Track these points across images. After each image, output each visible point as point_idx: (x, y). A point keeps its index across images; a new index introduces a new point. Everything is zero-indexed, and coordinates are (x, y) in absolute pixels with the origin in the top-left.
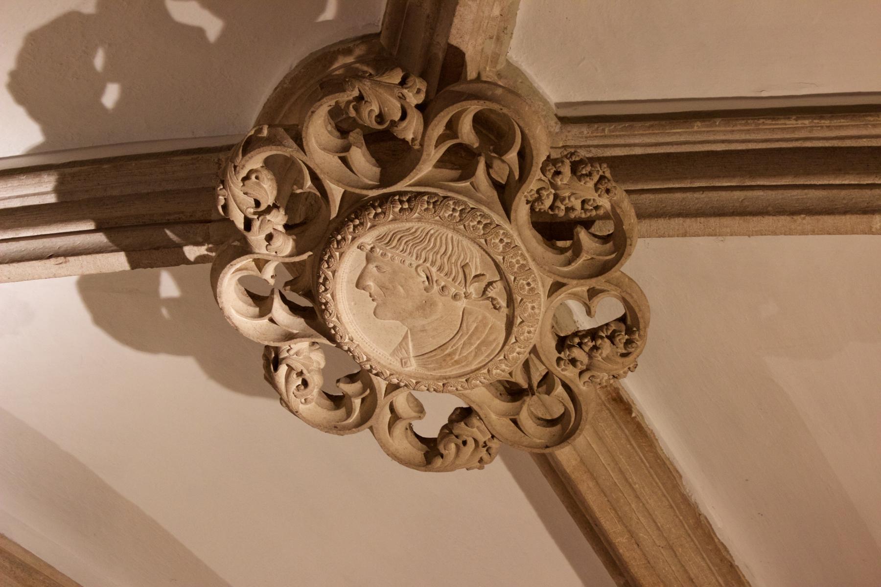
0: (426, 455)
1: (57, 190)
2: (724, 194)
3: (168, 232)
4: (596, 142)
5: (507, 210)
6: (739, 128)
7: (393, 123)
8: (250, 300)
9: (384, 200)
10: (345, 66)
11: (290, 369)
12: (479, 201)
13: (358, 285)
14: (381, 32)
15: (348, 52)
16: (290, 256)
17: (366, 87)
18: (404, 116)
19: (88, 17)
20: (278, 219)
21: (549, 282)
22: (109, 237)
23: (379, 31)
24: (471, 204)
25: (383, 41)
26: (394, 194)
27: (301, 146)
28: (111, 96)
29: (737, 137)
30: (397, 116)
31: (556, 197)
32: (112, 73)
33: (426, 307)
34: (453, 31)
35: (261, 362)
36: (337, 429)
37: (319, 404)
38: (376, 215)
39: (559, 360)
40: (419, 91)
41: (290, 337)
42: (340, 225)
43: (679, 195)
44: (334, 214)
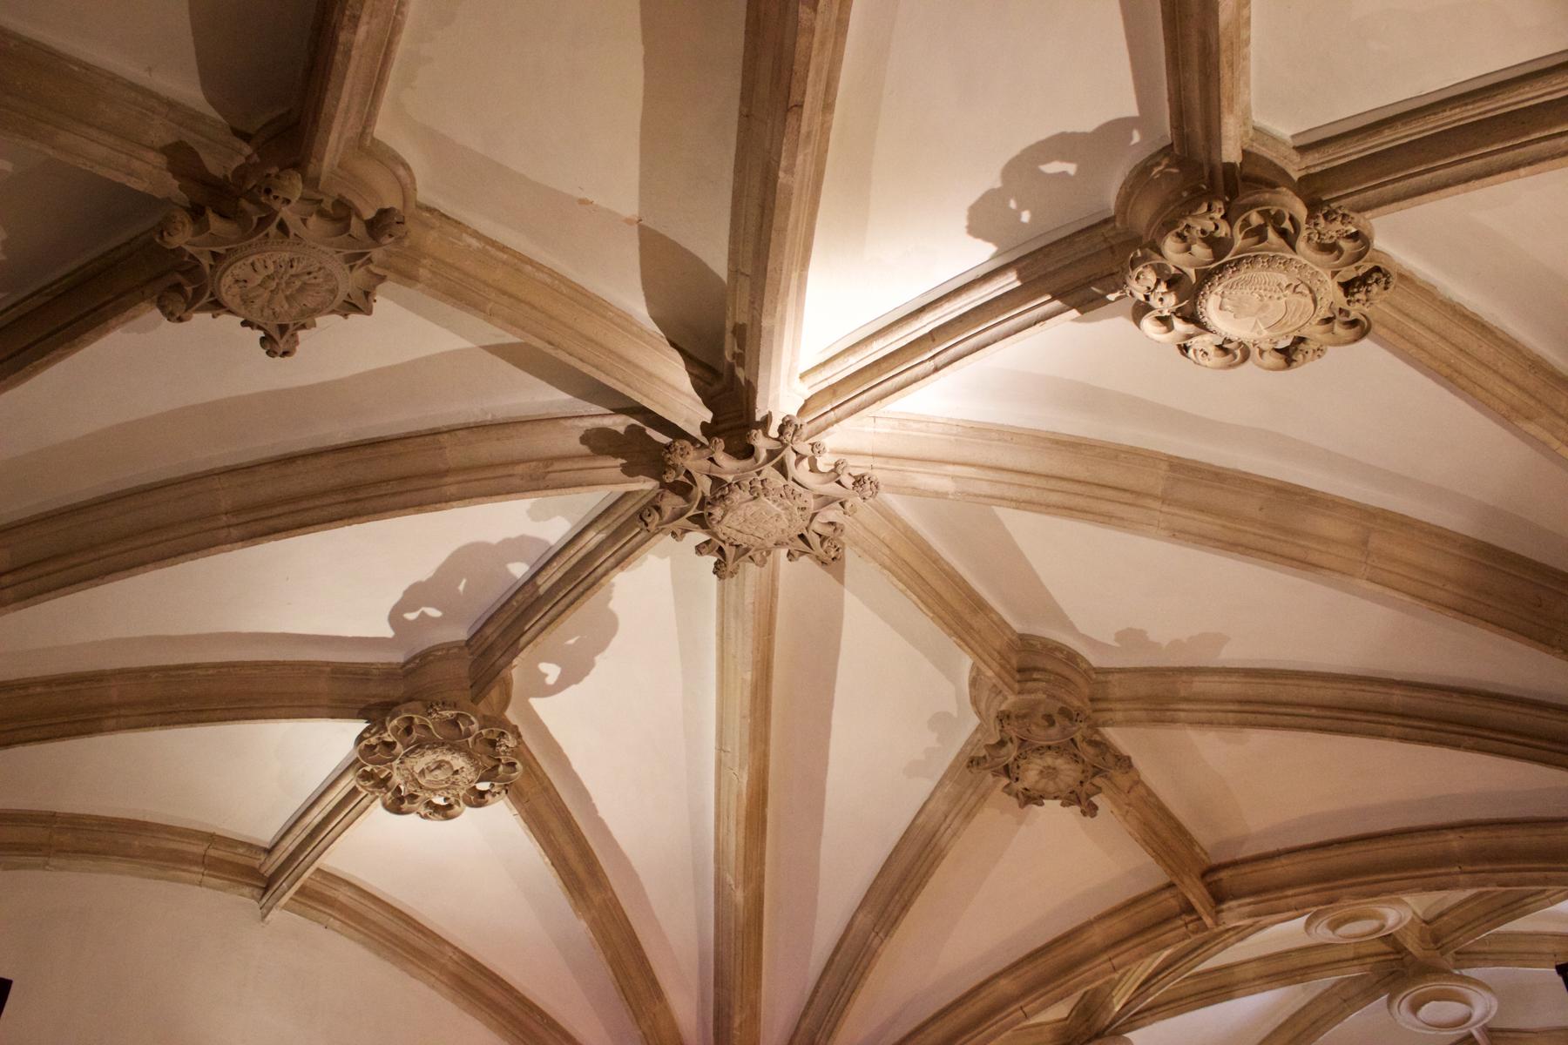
0: (1286, 360)
1: (1019, 278)
2: (1418, 178)
3: (1094, 289)
5: (1293, 248)
9: (1221, 269)
11: (1195, 351)
12: (1275, 250)
13: (1220, 309)
14: (1172, 144)
15: (1158, 164)
16: (1176, 304)
17: (1190, 221)
18: (1217, 228)
19: (999, 189)
20: (1163, 288)
23: (1170, 142)
24: (1271, 254)
25: (1176, 151)
27: (1161, 255)
29: (1414, 131)
30: (1213, 228)
31: (1319, 233)
32: (1021, 207)
34: (1224, 152)
35: (1178, 352)
36: (1231, 366)
38: (1220, 278)
39: (1349, 302)
41: (1189, 337)
43: (1390, 187)
44: (1194, 280)
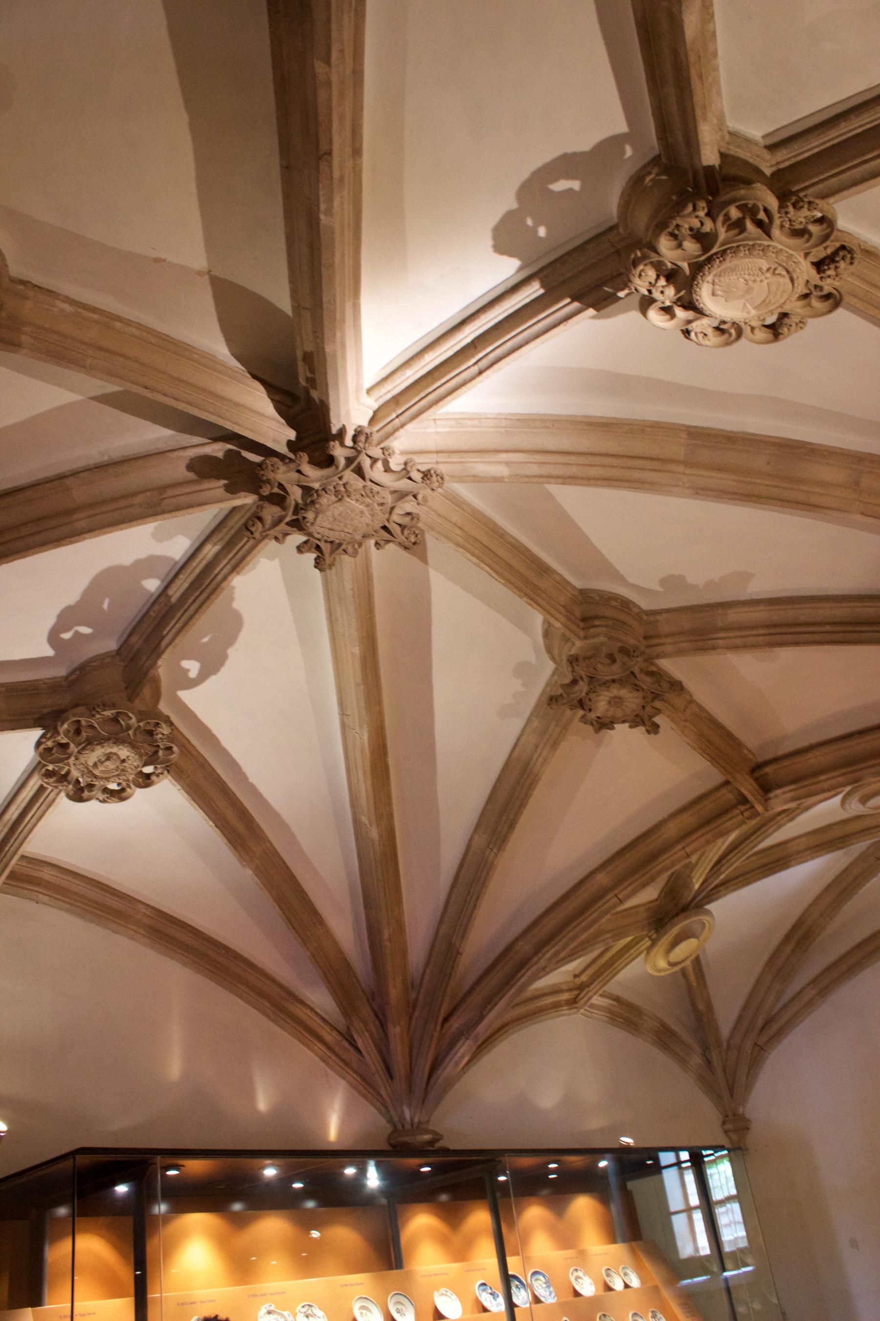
1: (542, 286)
3: (606, 289)
4: (793, 154)
5: (769, 235)
6: (866, 116)
7: (698, 229)
8: (663, 312)
9: (710, 260)
10: (651, 180)
11: (696, 334)
12: (754, 239)
15: (650, 173)
17: (678, 221)
20: (662, 282)
21: (802, 254)
22: (581, 303)
24: (751, 243)
26: (712, 255)
28: (542, 232)
31: (790, 221)
32: (537, 224)
33: (749, 290)
36: (728, 343)
37: (715, 336)
39: (821, 278)
40: (703, 208)
41: (689, 322)
42: (693, 277)
